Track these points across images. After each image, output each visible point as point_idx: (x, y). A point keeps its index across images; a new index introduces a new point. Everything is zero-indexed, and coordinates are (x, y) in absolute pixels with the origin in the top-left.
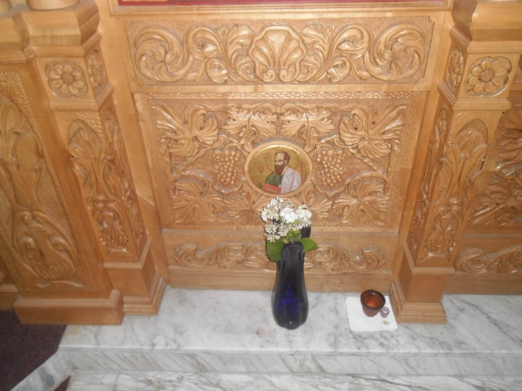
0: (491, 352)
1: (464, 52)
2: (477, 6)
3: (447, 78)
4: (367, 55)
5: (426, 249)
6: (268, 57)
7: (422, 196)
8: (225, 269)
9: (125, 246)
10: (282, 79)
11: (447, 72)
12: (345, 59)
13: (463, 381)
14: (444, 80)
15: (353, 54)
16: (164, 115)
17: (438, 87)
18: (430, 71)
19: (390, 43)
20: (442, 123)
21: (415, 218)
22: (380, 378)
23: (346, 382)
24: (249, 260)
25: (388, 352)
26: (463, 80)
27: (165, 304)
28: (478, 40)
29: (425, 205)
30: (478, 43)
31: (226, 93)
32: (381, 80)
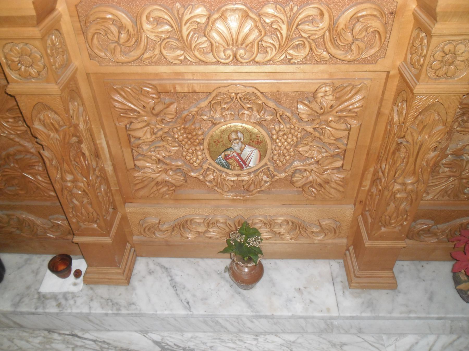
0: (155, 313)
1: (429, 35)
3: (408, 60)
4: (327, 33)
6: (112, 31)
10: (240, 59)
13: (145, 336)
18: (391, 51)
20: (402, 105)
21: (370, 194)
22: (73, 333)
23: (40, 336)
25: (62, 311)
26: (426, 62)
29: (381, 182)
31: (318, 64)
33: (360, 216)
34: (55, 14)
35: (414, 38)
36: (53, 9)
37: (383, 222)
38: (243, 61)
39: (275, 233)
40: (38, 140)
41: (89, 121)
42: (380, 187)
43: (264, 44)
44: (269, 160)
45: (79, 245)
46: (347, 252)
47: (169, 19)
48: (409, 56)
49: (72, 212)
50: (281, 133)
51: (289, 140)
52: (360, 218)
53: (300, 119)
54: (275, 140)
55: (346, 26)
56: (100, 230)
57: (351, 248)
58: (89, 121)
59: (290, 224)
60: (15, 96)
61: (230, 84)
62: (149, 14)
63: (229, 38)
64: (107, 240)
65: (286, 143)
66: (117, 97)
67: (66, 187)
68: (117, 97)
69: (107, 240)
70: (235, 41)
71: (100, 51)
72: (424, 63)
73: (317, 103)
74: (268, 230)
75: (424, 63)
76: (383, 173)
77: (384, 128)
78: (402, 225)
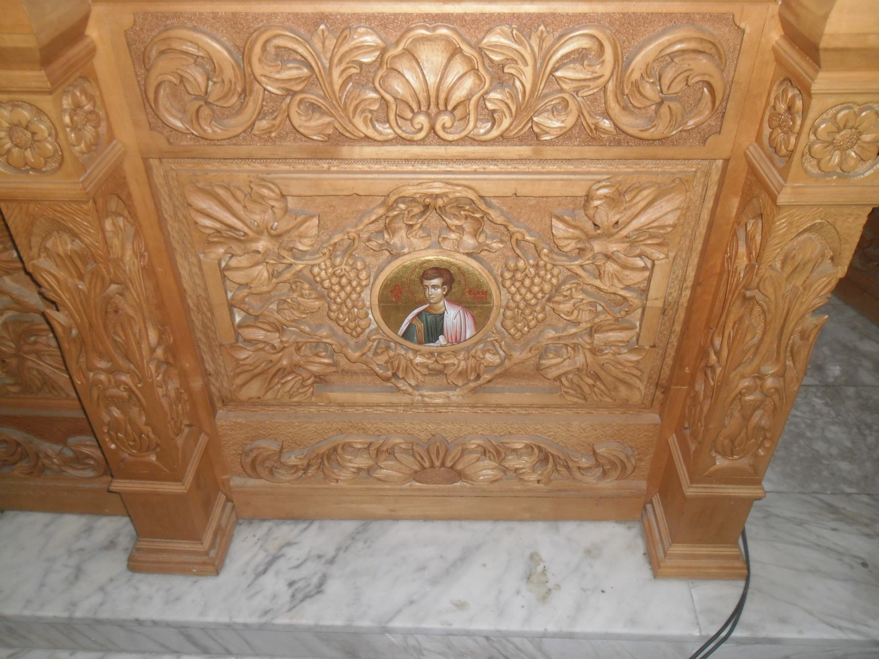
1: (806, 92)
7: (707, 355)
10: (441, 133)
11: (766, 125)
12: (566, 96)
14: (759, 139)
19: (657, 67)
33: (674, 435)
34: (86, 42)
35: (776, 98)
38: (450, 137)
39: (505, 470)
41: (146, 254)
42: (712, 383)
43: (490, 106)
47: (306, 54)
48: (767, 131)
49: (108, 432)
50: (519, 276)
51: (536, 289)
52: (673, 440)
55: (647, 72)
57: (656, 499)
58: (146, 254)
59: (536, 451)
62: (267, 41)
63: (422, 96)
65: (529, 296)
66: (204, 203)
67: (97, 383)
68: (204, 203)
70: (433, 93)
72: (796, 145)
75: (796, 145)
76: (718, 354)
77: (741, 461)
78: (756, 456)
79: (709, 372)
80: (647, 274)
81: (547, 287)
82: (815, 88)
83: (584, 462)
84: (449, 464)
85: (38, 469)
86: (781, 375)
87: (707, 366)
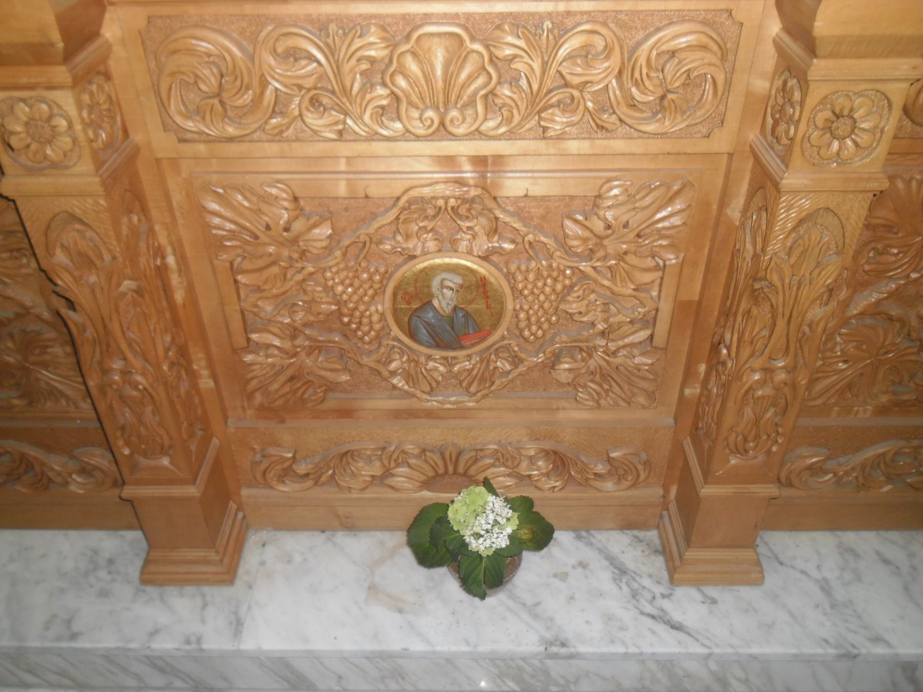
2: (107, 16)
5: (727, 451)
8: (350, 492)
9: (163, 451)
15: (587, 83)
16: (220, 205)
17: (751, 147)
24: (393, 475)
27: (251, 558)
28: (831, 55)
30: (831, 63)
32: (645, 133)
33: (688, 438)
36: (95, 34)
37: (732, 445)
40: (57, 289)
44: (508, 329)
45: (133, 505)
46: (665, 513)
53: (568, 251)
54: (521, 292)
56: (175, 470)
60: (15, 198)
61: (436, 181)
64: (192, 491)
69: (192, 491)
71: (187, 117)
73: (607, 237)
74: (508, 471)
76: (728, 348)
78: (769, 451)
79: (720, 368)
80: (660, 274)
81: (559, 287)
82: (812, 75)
83: (600, 468)
84: (461, 470)
85: (43, 482)
86: (791, 370)
87: (719, 363)
